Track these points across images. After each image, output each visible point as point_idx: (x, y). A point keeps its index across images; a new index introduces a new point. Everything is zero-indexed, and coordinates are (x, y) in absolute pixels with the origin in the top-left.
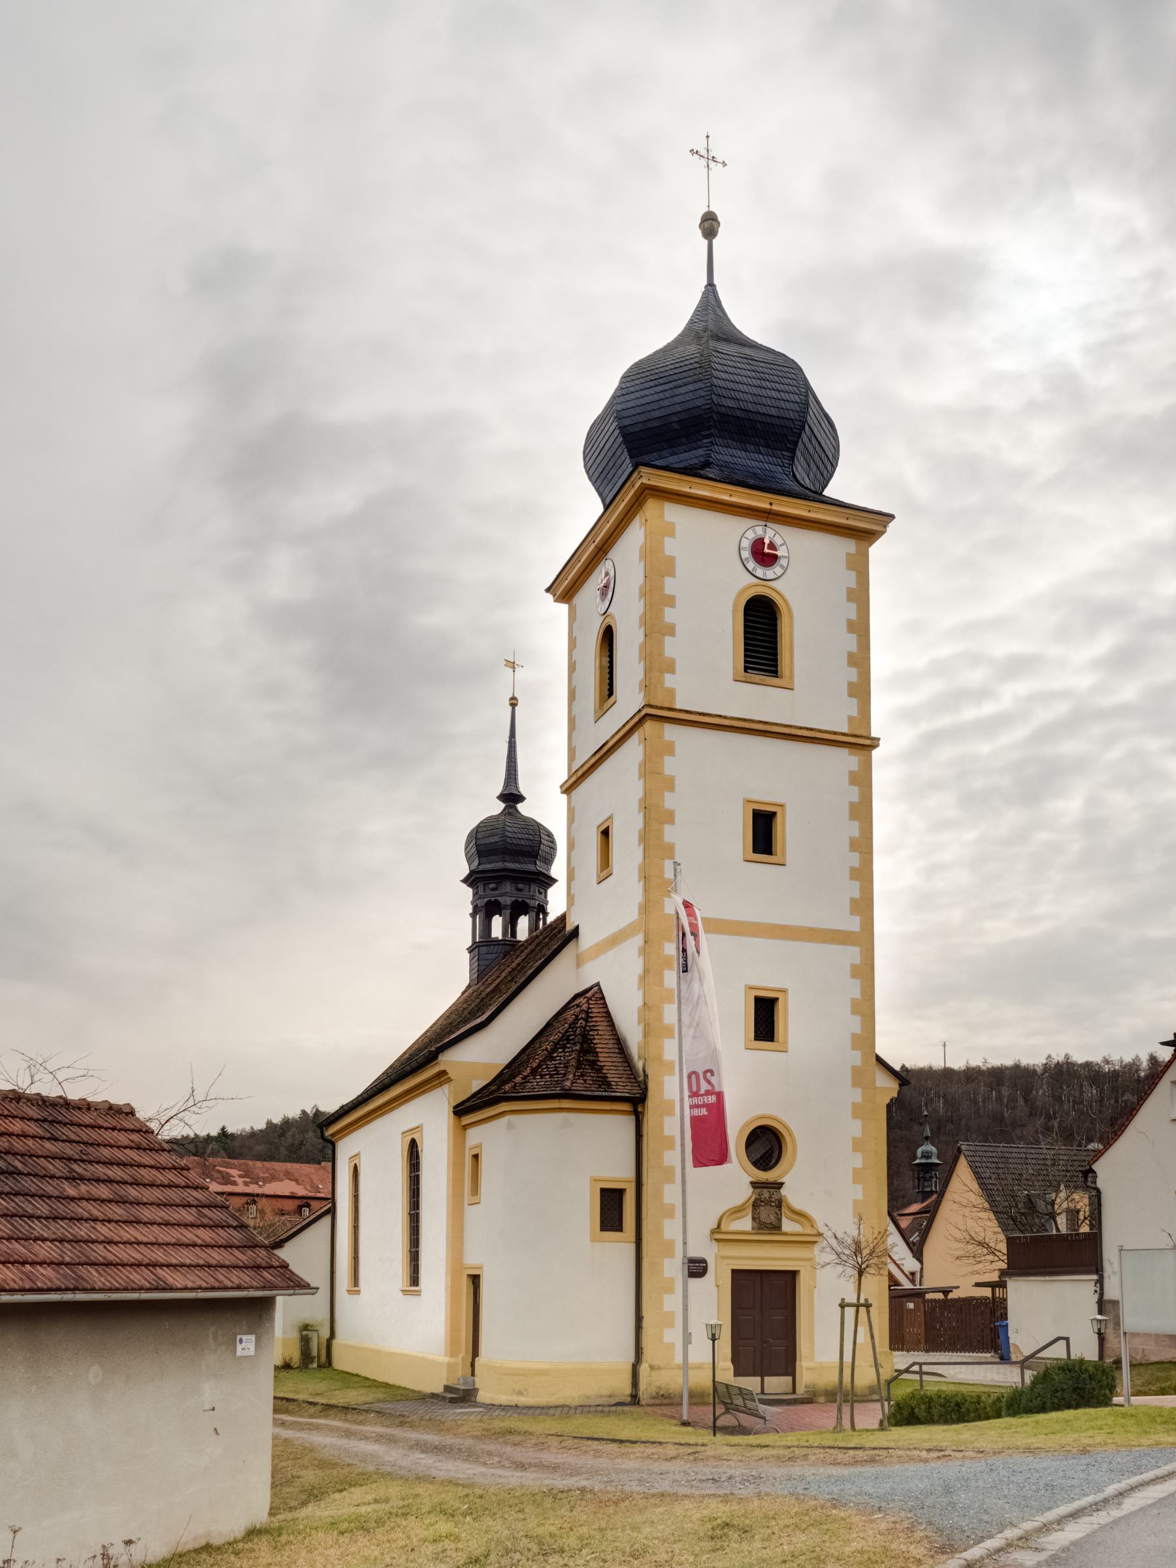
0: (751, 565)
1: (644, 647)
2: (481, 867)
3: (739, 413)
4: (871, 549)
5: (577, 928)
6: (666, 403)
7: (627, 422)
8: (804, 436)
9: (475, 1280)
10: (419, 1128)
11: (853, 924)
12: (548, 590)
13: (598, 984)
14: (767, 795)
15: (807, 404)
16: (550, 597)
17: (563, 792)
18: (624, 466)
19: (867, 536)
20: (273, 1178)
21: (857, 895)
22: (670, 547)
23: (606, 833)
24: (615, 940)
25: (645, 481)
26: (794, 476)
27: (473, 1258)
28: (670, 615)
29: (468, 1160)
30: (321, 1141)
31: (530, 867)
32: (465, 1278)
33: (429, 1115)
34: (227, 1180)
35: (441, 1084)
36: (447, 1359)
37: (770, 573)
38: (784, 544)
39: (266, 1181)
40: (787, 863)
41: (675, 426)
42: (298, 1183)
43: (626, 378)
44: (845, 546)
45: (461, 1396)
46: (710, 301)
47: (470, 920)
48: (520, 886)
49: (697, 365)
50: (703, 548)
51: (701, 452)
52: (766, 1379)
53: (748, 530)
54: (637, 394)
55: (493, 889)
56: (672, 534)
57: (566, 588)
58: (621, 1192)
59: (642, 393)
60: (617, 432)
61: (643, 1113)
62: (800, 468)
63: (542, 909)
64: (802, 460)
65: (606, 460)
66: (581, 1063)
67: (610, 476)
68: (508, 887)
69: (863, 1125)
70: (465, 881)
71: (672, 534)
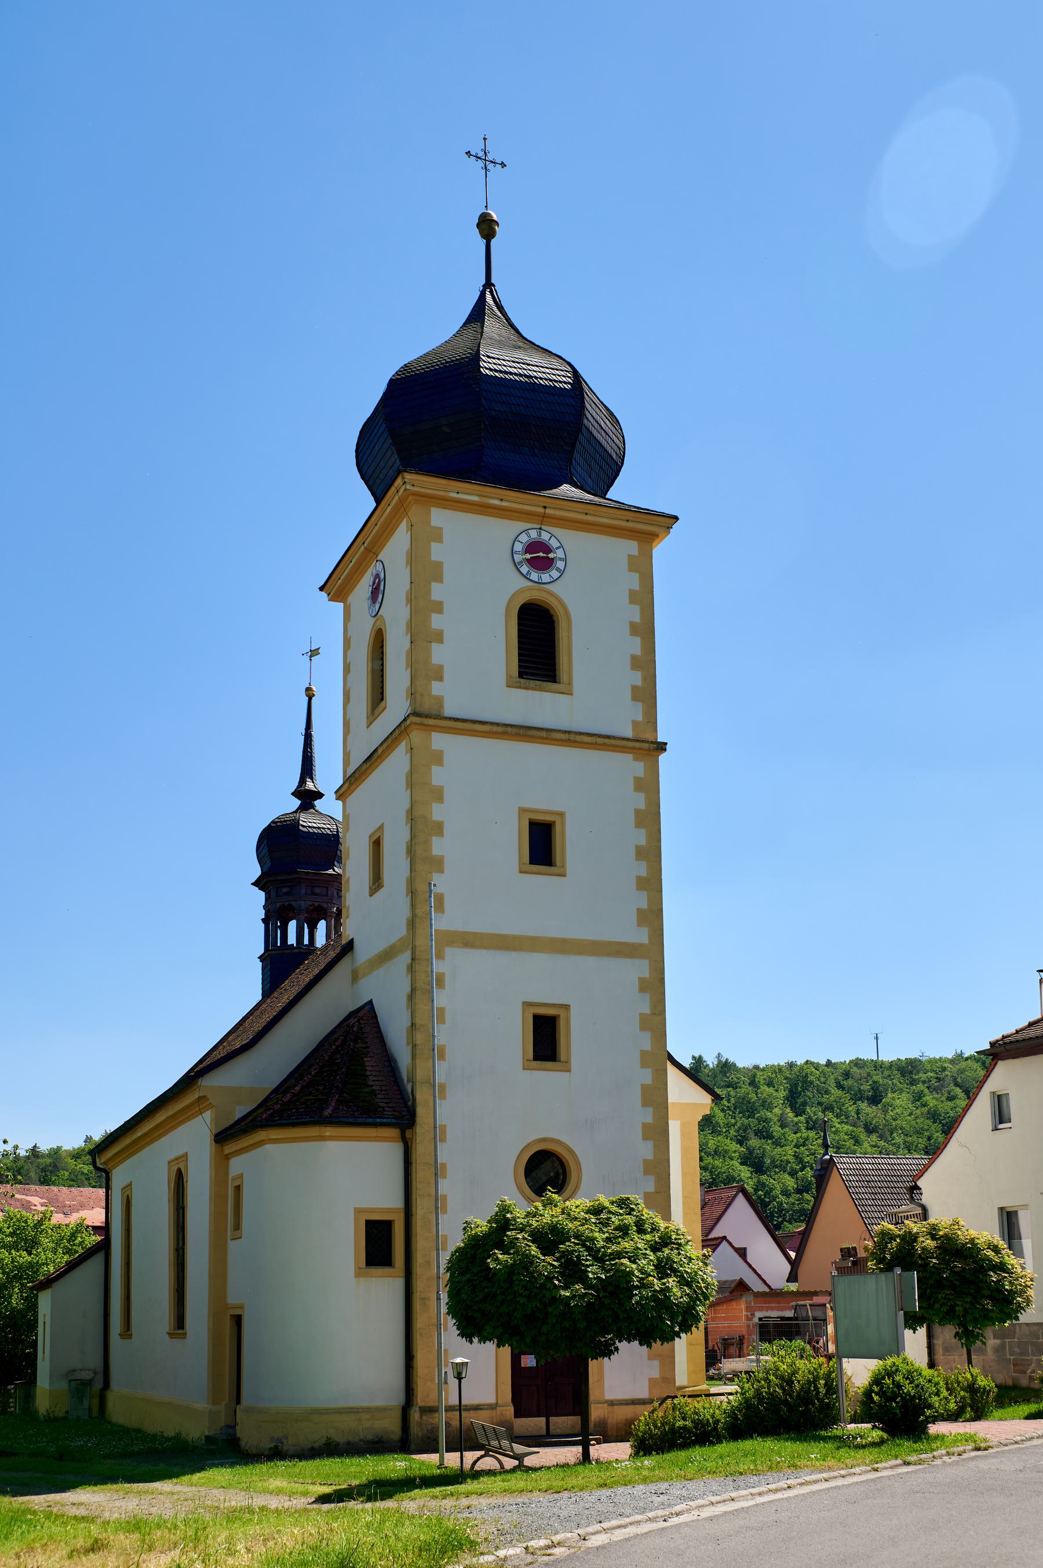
1: (411, 652)
9: (238, 1320)
11: (642, 936)
12: (321, 589)
13: (370, 1002)
14: (543, 802)
16: (323, 595)
24: (387, 956)
28: (436, 621)
29: (231, 1192)
30: (91, 1168)
37: (546, 578)
50: (474, 549)
52: (552, 1419)
56: (439, 539)
57: (335, 587)
61: (411, 1139)
62: (579, 469)
69: (655, 1146)
71: (439, 539)
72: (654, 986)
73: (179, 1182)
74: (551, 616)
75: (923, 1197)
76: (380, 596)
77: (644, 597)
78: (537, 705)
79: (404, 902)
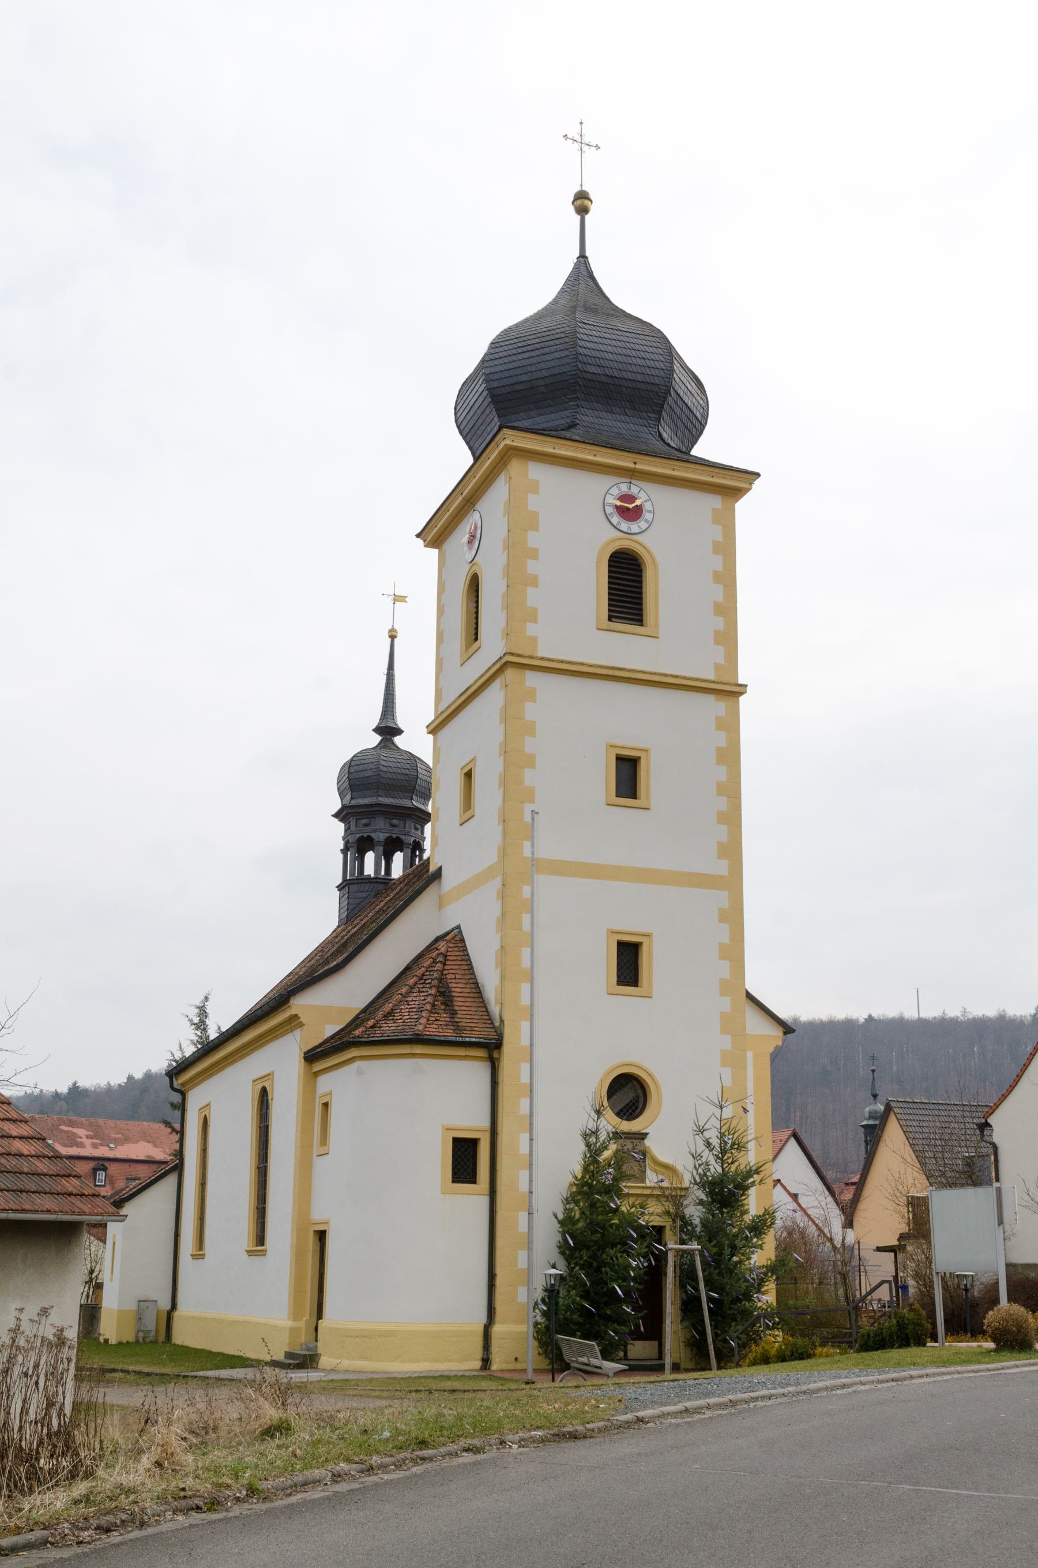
0: (616, 519)
1: (507, 596)
2: (353, 802)
3: (603, 379)
4: (737, 505)
5: (440, 868)
6: (534, 368)
7: (495, 384)
8: (670, 399)
9: (322, 1235)
10: (270, 1076)
11: (722, 868)
12: (418, 536)
13: (458, 927)
15: (672, 370)
16: (420, 541)
17: (430, 733)
18: (493, 423)
19: (737, 493)
20: (126, 1140)
21: (725, 839)
22: (534, 502)
23: (469, 775)
25: (508, 442)
26: (660, 435)
27: (320, 1213)
29: (318, 1109)
31: (407, 803)
32: (312, 1233)
33: (281, 1060)
34: (72, 1140)
35: (291, 1030)
36: (289, 1323)
37: (634, 527)
38: (649, 499)
39: (118, 1142)
40: (652, 806)
41: (542, 389)
42: (155, 1146)
43: (494, 345)
44: (715, 501)
45: (305, 1360)
46: (582, 273)
47: (341, 856)
48: (395, 822)
49: (563, 335)
50: (567, 508)
51: (566, 413)
53: (612, 489)
54: (506, 360)
55: (366, 825)
58: (474, 1143)
59: (510, 359)
60: (485, 393)
61: (498, 1059)
63: (418, 846)
64: (668, 420)
65: (476, 417)
66: (442, 1010)
67: (479, 432)
68: (380, 822)
70: (336, 816)
72: (733, 916)
73: (264, 1100)
74: (639, 565)
75: (994, 1134)
76: (477, 543)
77: (726, 548)
78: (624, 648)
79: (495, 832)
